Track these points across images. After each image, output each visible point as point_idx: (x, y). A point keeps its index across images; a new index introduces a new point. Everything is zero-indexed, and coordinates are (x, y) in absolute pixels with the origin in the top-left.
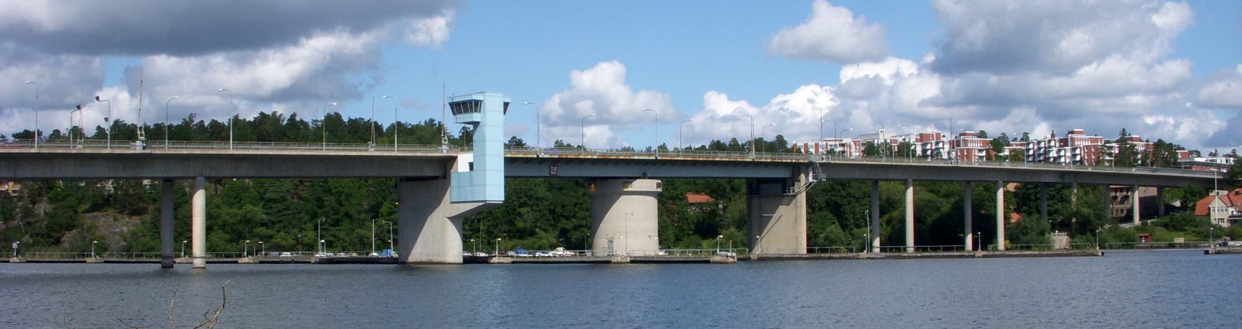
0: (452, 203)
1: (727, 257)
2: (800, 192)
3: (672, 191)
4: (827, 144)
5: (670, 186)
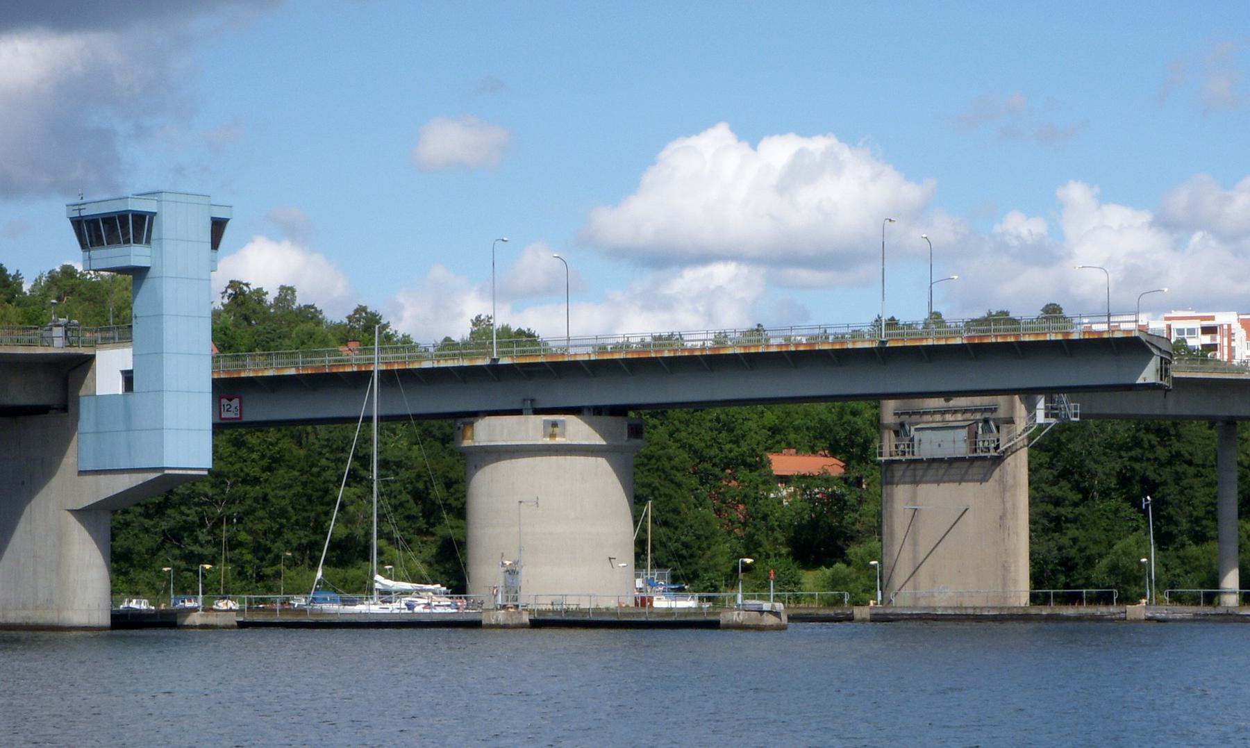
0: (81, 473)
1: (761, 612)
2: (1012, 450)
3: (728, 446)
4: (1169, 327)
5: (724, 434)
